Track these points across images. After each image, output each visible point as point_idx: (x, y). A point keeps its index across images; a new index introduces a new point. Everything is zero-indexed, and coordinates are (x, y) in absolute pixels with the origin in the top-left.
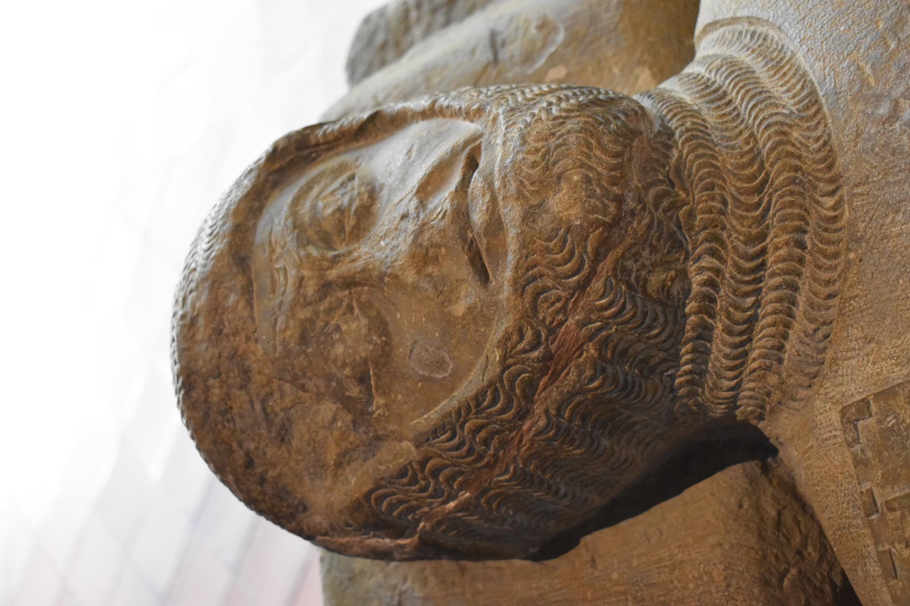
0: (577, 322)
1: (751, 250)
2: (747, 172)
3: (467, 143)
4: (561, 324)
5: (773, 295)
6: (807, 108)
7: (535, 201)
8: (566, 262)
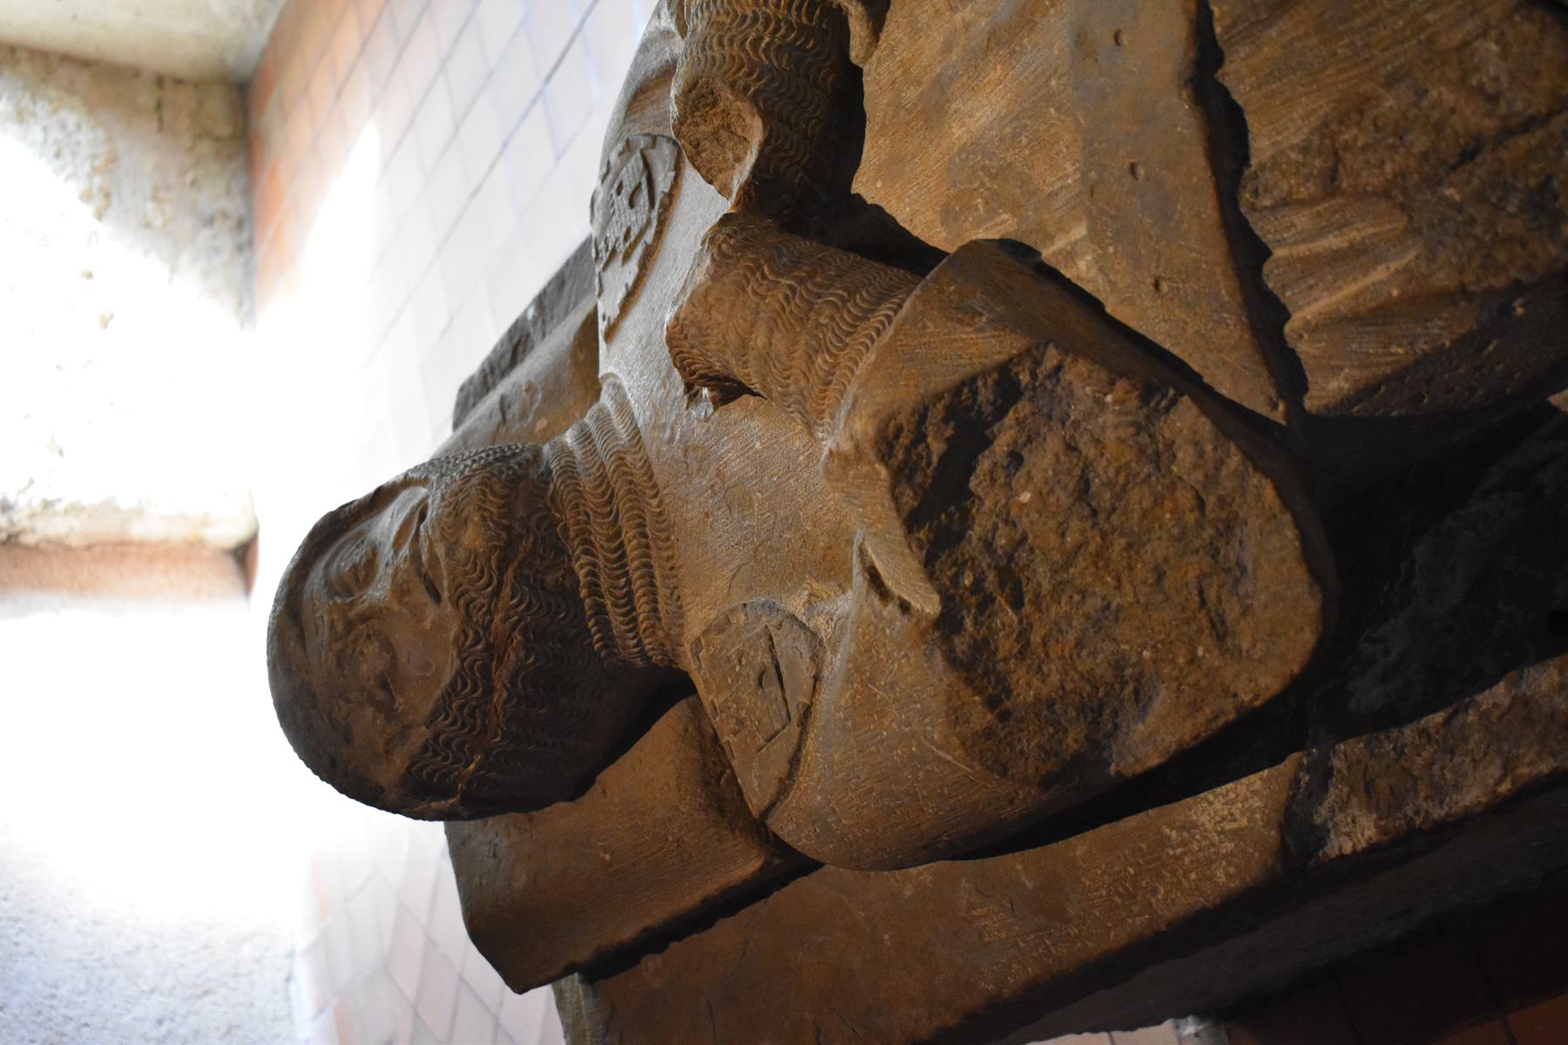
0: (501, 619)
1: (613, 546)
2: (599, 491)
3: (419, 504)
4: (491, 622)
5: (637, 574)
6: (633, 438)
7: (452, 539)
8: (480, 578)
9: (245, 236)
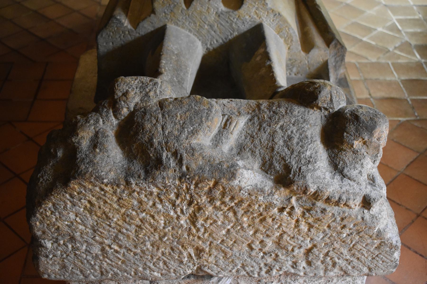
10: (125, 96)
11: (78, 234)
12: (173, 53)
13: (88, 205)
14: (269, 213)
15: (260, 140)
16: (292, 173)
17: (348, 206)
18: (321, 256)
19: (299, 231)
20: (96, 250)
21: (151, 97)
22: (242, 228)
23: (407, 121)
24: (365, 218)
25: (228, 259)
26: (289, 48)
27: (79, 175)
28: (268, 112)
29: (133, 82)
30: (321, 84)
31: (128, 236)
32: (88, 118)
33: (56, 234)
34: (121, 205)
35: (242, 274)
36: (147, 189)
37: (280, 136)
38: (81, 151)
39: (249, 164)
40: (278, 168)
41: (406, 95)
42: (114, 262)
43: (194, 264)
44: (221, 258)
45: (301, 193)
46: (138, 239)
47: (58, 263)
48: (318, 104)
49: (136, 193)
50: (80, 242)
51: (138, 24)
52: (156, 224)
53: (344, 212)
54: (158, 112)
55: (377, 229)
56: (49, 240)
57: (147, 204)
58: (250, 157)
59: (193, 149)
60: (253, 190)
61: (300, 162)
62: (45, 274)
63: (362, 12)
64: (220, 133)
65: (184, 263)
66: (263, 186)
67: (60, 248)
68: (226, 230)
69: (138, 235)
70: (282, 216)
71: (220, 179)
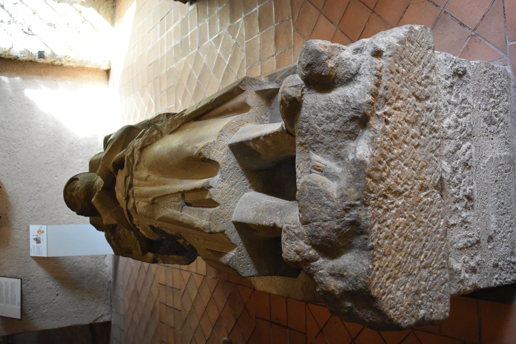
9: (114, 5)
10: (299, 252)
11: (413, 288)
12: (256, 215)
13: (390, 280)
14: (390, 132)
15: (330, 142)
16: (357, 115)
17: (381, 69)
18: (421, 88)
19: (402, 107)
20: (425, 273)
21: (299, 231)
22: (402, 153)
23: (293, 25)
24: (390, 54)
25: (427, 164)
26: (247, 122)
27: (367, 289)
28: (307, 137)
29: (287, 247)
30: (283, 95)
31: (413, 247)
32: (318, 282)
33: (414, 306)
34: (389, 253)
35: (438, 152)
36: (376, 232)
37: (327, 126)
38: (347, 287)
39: (351, 150)
40: (353, 127)
41: (273, 27)
42: (434, 258)
43: (433, 192)
44: (427, 170)
45: (373, 107)
46: (415, 239)
47: (437, 304)
48: (299, 97)
49: (380, 242)
50: (419, 286)
51: (233, 244)
52: (402, 224)
53: (386, 72)
54: (312, 226)
55: (398, 45)
56: (419, 312)
57: (387, 232)
58: (345, 149)
59: (342, 196)
60: (372, 146)
61: (347, 109)
62: (445, 315)
63: (205, 65)
64: (326, 175)
65: (432, 200)
66: (368, 138)
67: (425, 303)
68: (404, 167)
69: (412, 239)
70: (392, 122)
71: (365, 173)
